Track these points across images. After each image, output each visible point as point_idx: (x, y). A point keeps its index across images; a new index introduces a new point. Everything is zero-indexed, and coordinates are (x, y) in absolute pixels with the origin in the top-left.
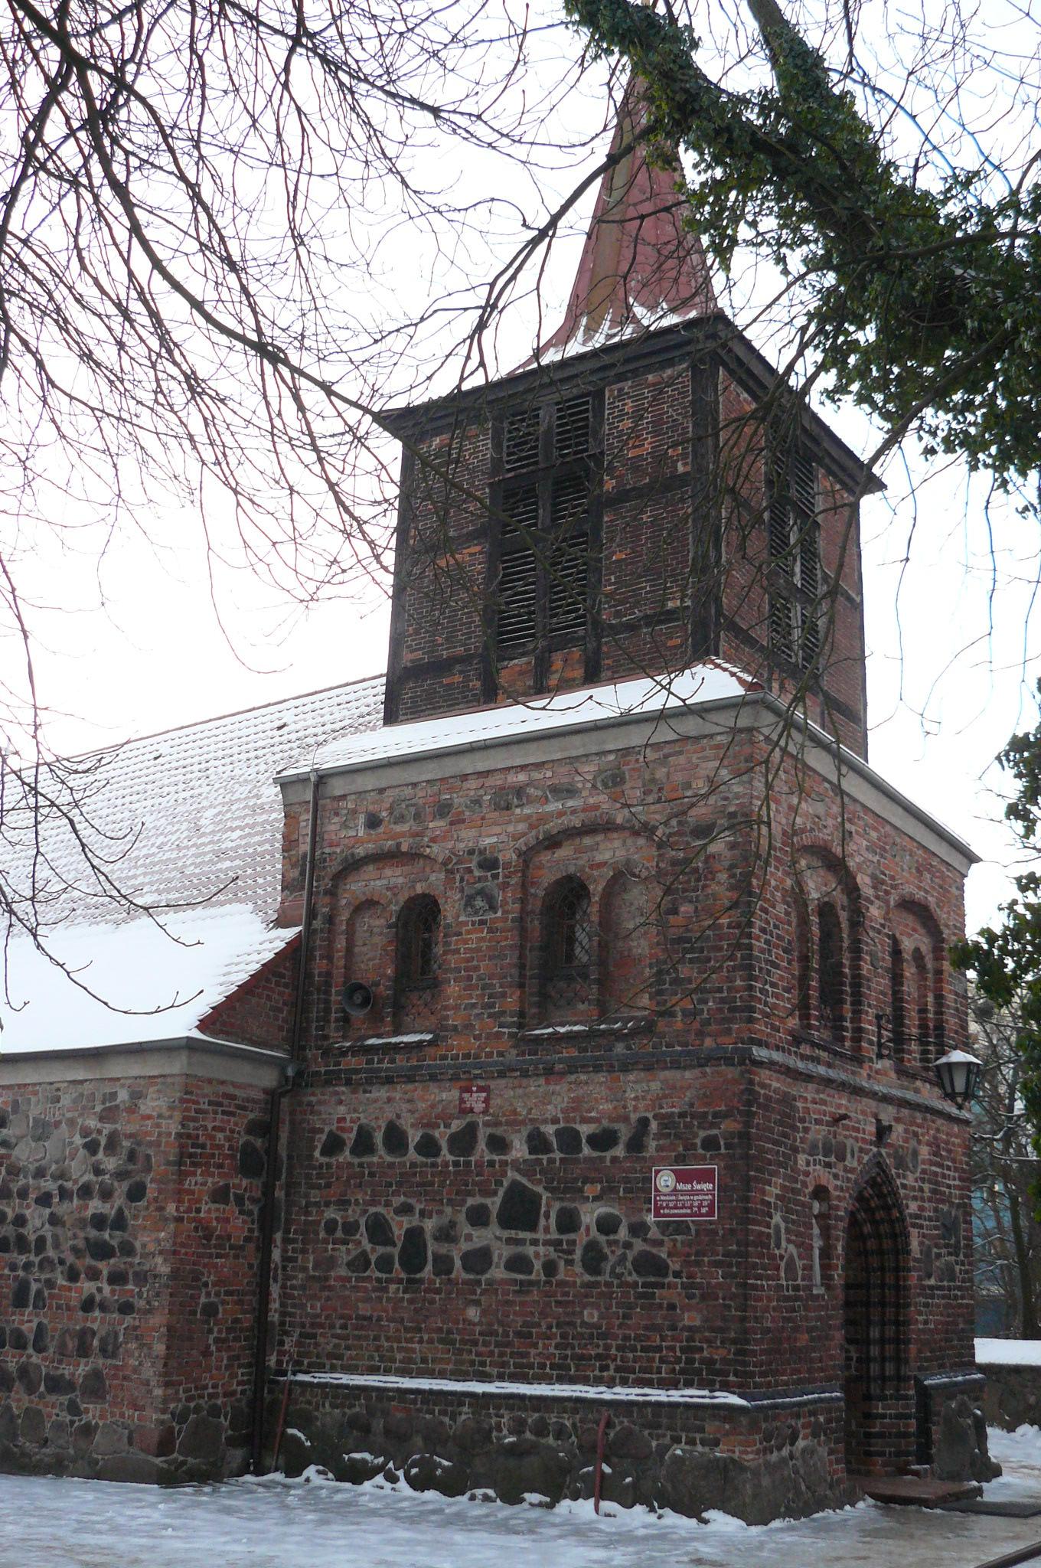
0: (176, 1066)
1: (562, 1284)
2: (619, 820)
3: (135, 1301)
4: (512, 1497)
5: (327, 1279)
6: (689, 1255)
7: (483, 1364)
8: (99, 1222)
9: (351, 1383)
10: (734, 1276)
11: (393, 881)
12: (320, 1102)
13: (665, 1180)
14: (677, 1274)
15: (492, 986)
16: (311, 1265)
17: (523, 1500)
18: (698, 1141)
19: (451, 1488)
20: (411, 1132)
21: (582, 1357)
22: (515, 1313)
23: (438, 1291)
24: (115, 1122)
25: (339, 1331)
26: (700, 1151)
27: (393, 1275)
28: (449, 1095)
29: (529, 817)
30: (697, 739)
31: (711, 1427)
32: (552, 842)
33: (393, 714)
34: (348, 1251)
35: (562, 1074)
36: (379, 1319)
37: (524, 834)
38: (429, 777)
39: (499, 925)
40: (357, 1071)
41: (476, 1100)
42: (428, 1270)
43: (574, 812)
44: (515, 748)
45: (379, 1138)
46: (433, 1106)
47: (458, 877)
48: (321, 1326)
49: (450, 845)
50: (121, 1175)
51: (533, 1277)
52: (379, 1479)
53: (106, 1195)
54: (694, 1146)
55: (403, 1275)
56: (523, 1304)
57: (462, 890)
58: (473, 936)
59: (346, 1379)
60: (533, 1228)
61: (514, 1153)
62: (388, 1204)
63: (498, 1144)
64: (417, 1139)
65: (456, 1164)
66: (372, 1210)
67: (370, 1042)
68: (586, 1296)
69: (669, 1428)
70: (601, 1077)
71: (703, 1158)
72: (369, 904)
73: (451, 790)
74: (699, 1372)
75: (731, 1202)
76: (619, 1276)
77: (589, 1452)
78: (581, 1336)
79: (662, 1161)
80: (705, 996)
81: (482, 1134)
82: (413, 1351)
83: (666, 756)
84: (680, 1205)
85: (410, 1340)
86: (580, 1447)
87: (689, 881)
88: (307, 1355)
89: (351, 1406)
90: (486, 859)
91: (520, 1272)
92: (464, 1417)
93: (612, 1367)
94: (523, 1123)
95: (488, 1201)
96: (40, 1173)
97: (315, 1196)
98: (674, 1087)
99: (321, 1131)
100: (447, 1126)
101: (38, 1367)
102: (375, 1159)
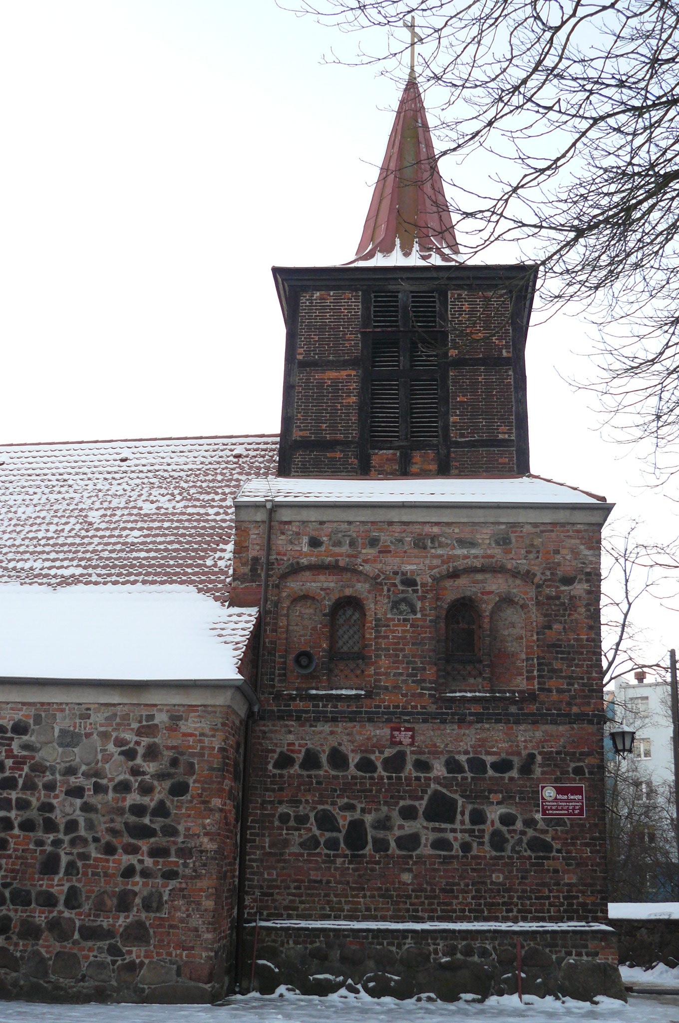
0: (221, 699)
1: (475, 857)
2: (509, 566)
3: (180, 870)
4: (450, 997)
5: (282, 854)
6: (567, 839)
7: (417, 911)
8: (138, 810)
9: (310, 926)
10: (598, 852)
11: (325, 585)
12: (271, 732)
13: (549, 793)
14: (559, 851)
15: (415, 662)
16: (267, 845)
17: (460, 998)
18: (570, 769)
19: (401, 993)
20: (351, 756)
21: (492, 904)
22: (441, 877)
23: (378, 863)
24: (155, 737)
25: (294, 891)
26: (572, 775)
27: (340, 852)
28: (383, 732)
29: (442, 556)
30: (563, 525)
31: (592, 945)
32: (455, 575)
33: (284, 471)
34: (300, 836)
35: (471, 723)
36: (328, 882)
37: (438, 567)
38: (363, 519)
39: (420, 623)
40: (307, 712)
41: (404, 737)
42: (369, 849)
43: (476, 557)
44: (433, 510)
45: (324, 758)
46: (368, 739)
47: (385, 588)
48: (278, 887)
49: (379, 566)
50: (161, 776)
51: (453, 853)
52: (343, 991)
53: (146, 790)
54: (567, 772)
55: (347, 852)
56: (445, 871)
57: (389, 597)
58: (400, 629)
59: (303, 924)
60: (452, 820)
61: (435, 771)
62: (334, 804)
63: (423, 766)
64: (356, 760)
65: (389, 778)
66: (320, 807)
67: (314, 692)
68: (494, 865)
69: (564, 946)
70: (500, 726)
71: (575, 780)
72: (305, 597)
73: (381, 530)
74: (577, 911)
75: (593, 807)
76: (518, 852)
77: (506, 963)
78: (491, 890)
79: (545, 780)
80: (573, 681)
81: (410, 759)
82: (359, 903)
83: (542, 532)
84: (560, 808)
85: (357, 896)
86: (500, 962)
87: (559, 610)
88: (267, 908)
89: (312, 943)
90: (407, 579)
91: (443, 850)
92: (407, 946)
93: (515, 910)
94: (442, 753)
95: (416, 803)
96: (71, 771)
97: (269, 796)
98: (552, 736)
99: (274, 751)
100: (381, 752)
101: (72, 921)
102: (321, 773)
